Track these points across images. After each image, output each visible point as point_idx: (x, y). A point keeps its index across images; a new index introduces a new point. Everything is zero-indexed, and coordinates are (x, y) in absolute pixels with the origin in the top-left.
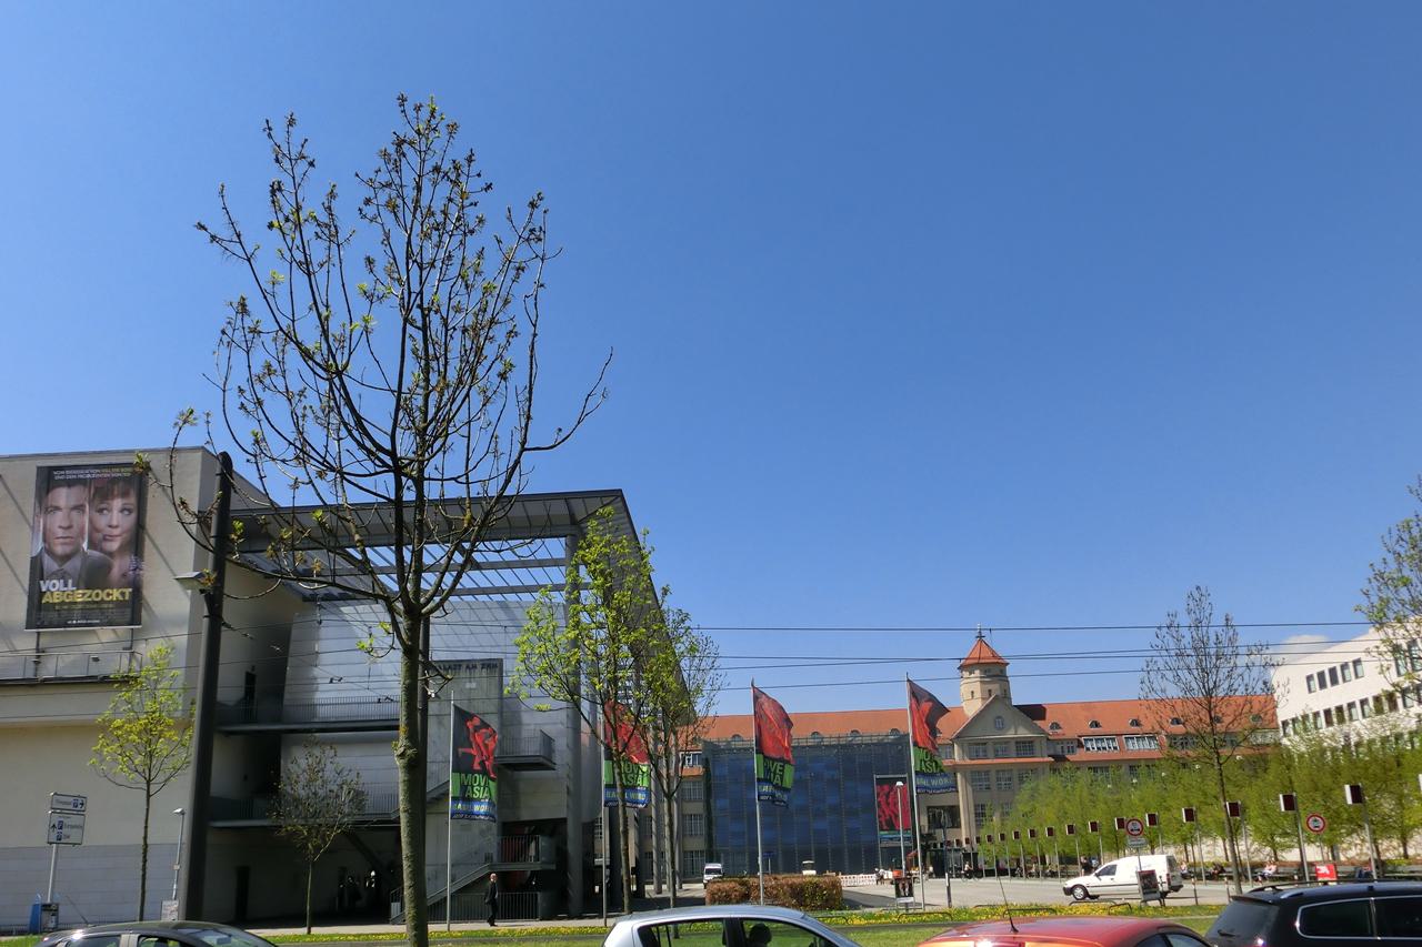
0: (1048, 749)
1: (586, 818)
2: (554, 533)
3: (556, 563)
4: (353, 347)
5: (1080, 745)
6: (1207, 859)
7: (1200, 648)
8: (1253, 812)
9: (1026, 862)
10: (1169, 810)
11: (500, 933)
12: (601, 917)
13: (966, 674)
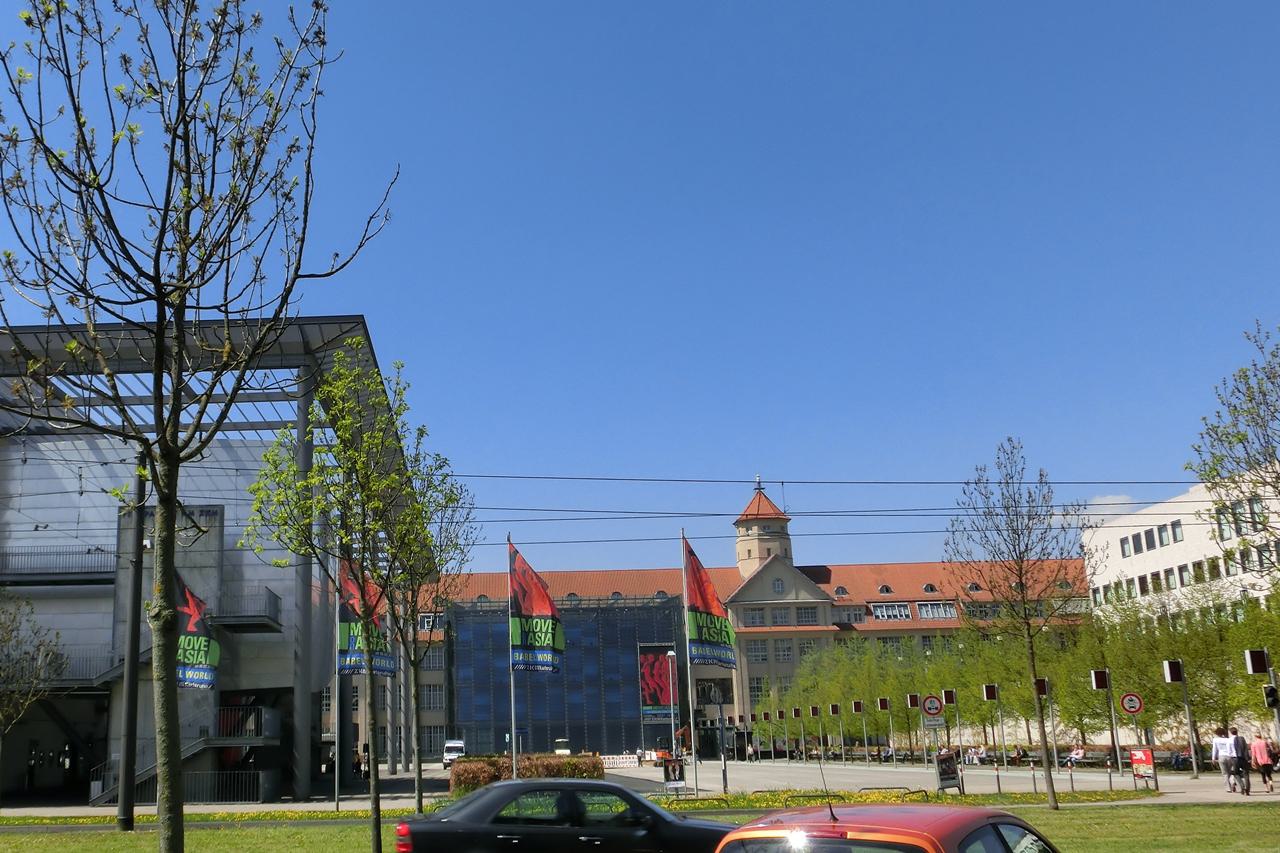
0: (833, 615)
1: (315, 690)
2: (285, 363)
3: (287, 397)
4: (109, 163)
5: (869, 612)
6: (1009, 741)
7: (1011, 507)
8: (1061, 689)
9: (806, 743)
10: (967, 687)
11: (217, 817)
12: (331, 799)
13: (742, 530)
